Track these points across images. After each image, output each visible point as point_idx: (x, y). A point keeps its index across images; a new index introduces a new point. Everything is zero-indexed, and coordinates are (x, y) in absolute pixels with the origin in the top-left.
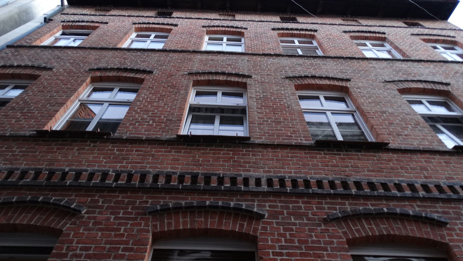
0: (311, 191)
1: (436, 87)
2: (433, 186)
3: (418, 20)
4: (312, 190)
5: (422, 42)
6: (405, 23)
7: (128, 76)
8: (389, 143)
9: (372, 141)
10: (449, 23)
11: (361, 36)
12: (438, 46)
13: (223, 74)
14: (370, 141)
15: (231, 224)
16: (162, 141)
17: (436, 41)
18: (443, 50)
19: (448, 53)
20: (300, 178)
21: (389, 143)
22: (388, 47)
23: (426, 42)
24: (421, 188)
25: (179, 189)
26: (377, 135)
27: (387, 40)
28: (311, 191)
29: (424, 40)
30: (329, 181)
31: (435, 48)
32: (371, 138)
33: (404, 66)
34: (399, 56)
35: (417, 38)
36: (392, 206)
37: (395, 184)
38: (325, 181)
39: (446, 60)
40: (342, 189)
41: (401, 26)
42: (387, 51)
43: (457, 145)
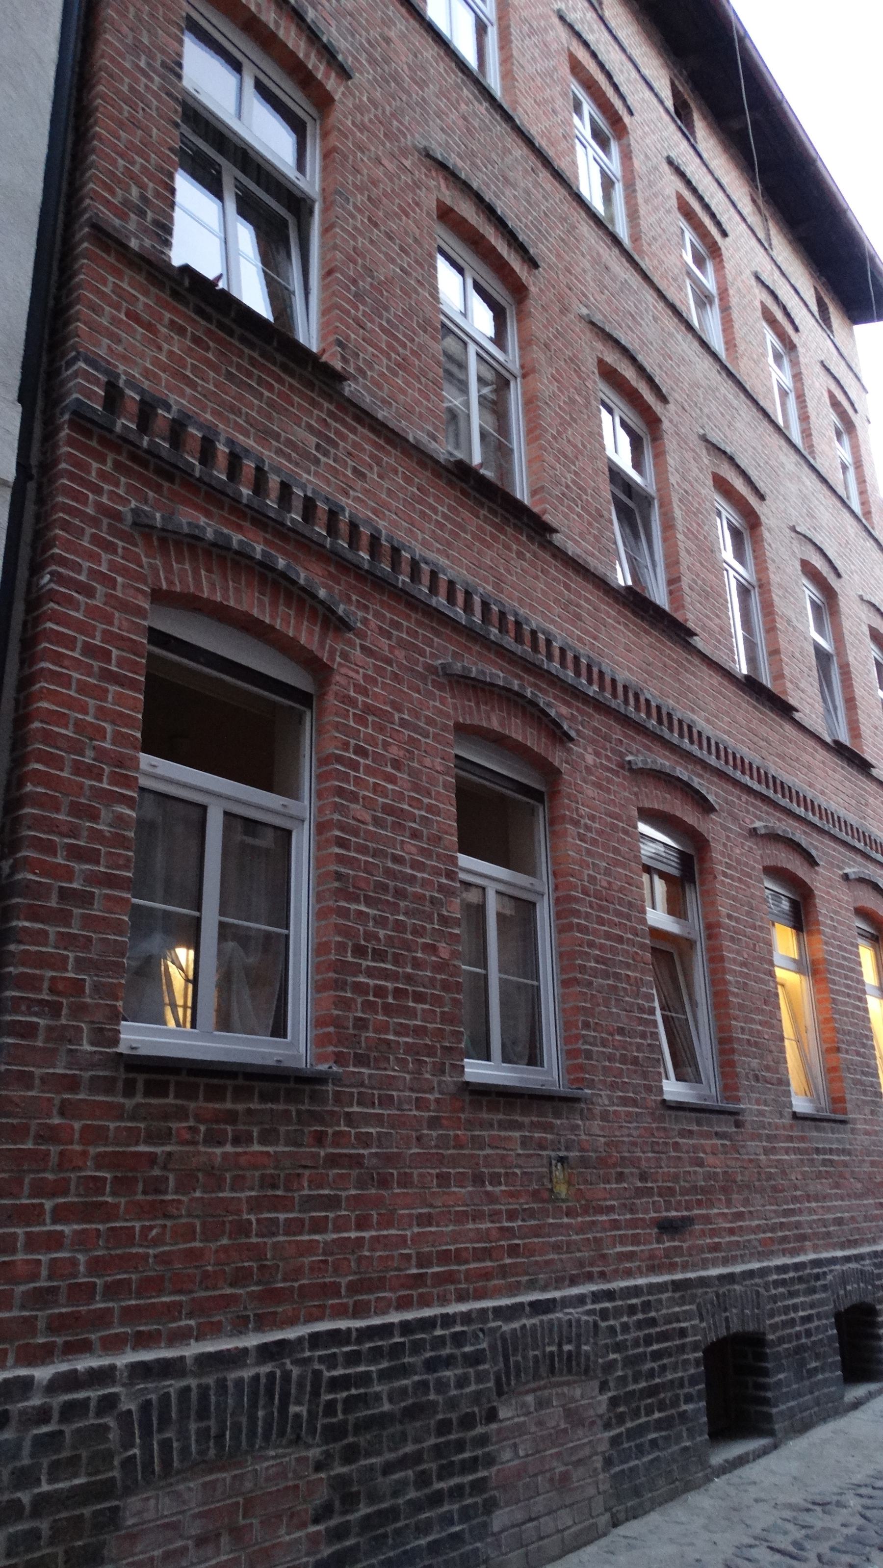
0: (145, 442)
1: (307, 55)
3: (700, 109)
4: (152, 442)
5: (674, 202)
6: (676, 94)
8: (555, 531)
10: (852, 335)
12: (588, 107)
13: (312, 35)
17: (590, 86)
18: (587, 132)
20: (303, 487)
21: (555, 531)
22: (615, 166)
26: (778, 676)
28: (145, 442)
29: (832, 396)
30: (142, 402)
31: (577, 108)
32: (522, 492)
33: (851, 527)
36: (94, 474)
38: (195, 432)
39: (568, 173)
40: (134, 427)
41: (656, 85)
42: (478, 18)
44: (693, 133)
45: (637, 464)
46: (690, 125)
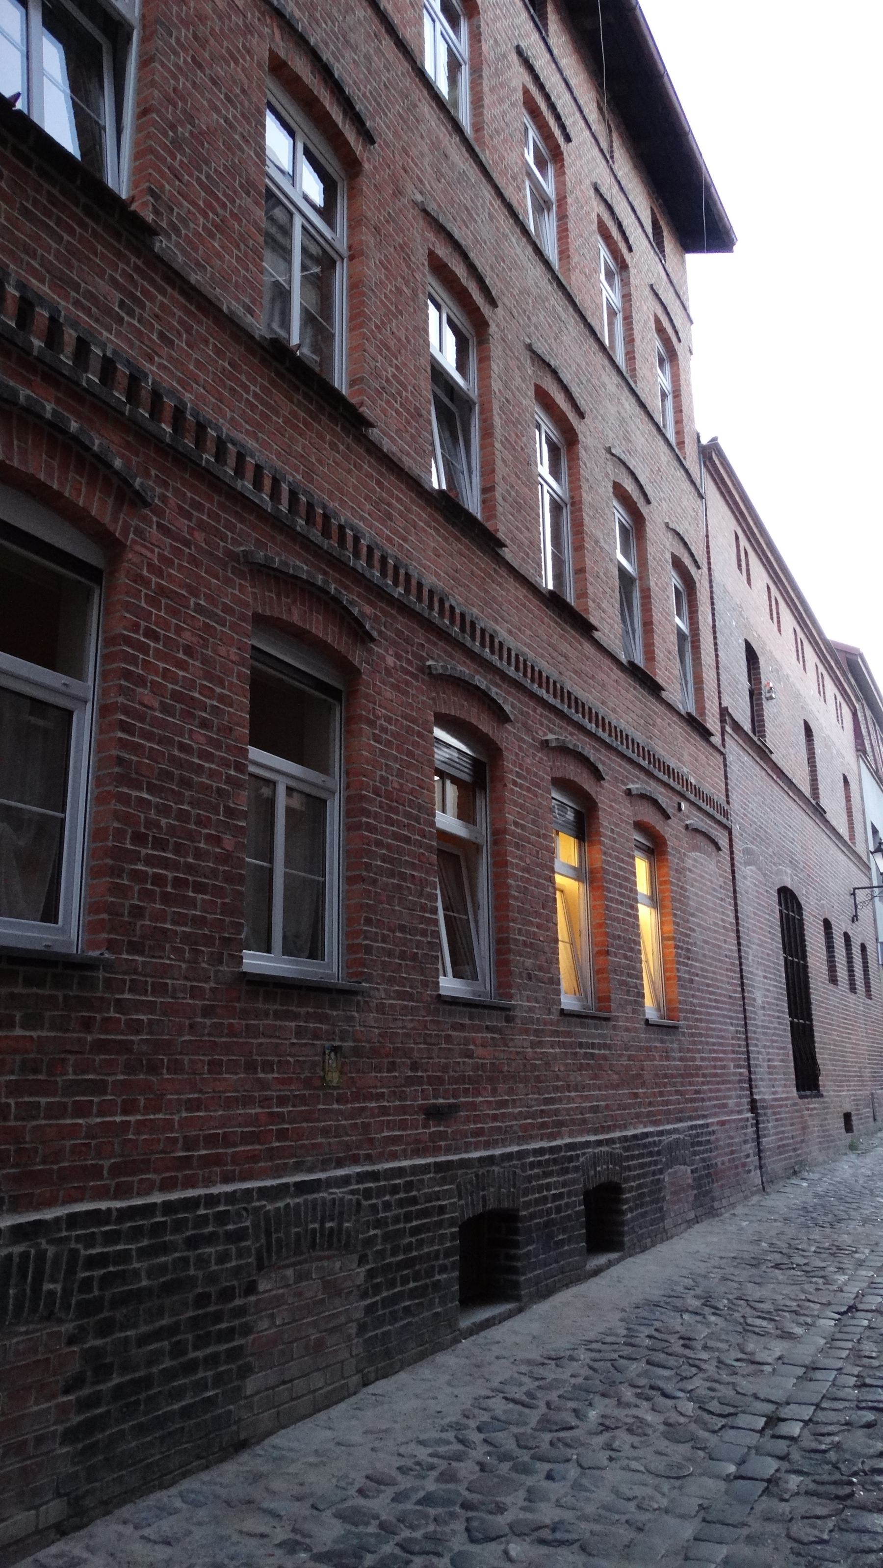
2: (74, 334)
7: (464, 281)
9: (117, 192)
10: (683, 262)
11: (615, 243)
14: (110, 185)
15: (83, 490)
16: (422, 487)
19: (438, 26)
20: (103, 346)
23: (525, 103)
24: (125, 382)
25: (123, 414)
26: (582, 594)
27: (624, 274)
29: (658, 321)
30: (219, 438)
32: (340, 381)
34: (465, 117)
35: (598, 208)
37: (219, 438)
43: (26, 112)
44: (545, 25)
45: (461, 366)
46: (543, 17)
